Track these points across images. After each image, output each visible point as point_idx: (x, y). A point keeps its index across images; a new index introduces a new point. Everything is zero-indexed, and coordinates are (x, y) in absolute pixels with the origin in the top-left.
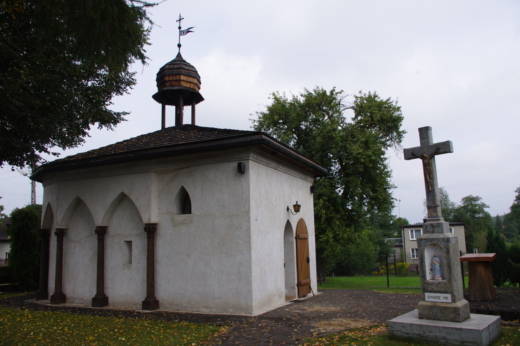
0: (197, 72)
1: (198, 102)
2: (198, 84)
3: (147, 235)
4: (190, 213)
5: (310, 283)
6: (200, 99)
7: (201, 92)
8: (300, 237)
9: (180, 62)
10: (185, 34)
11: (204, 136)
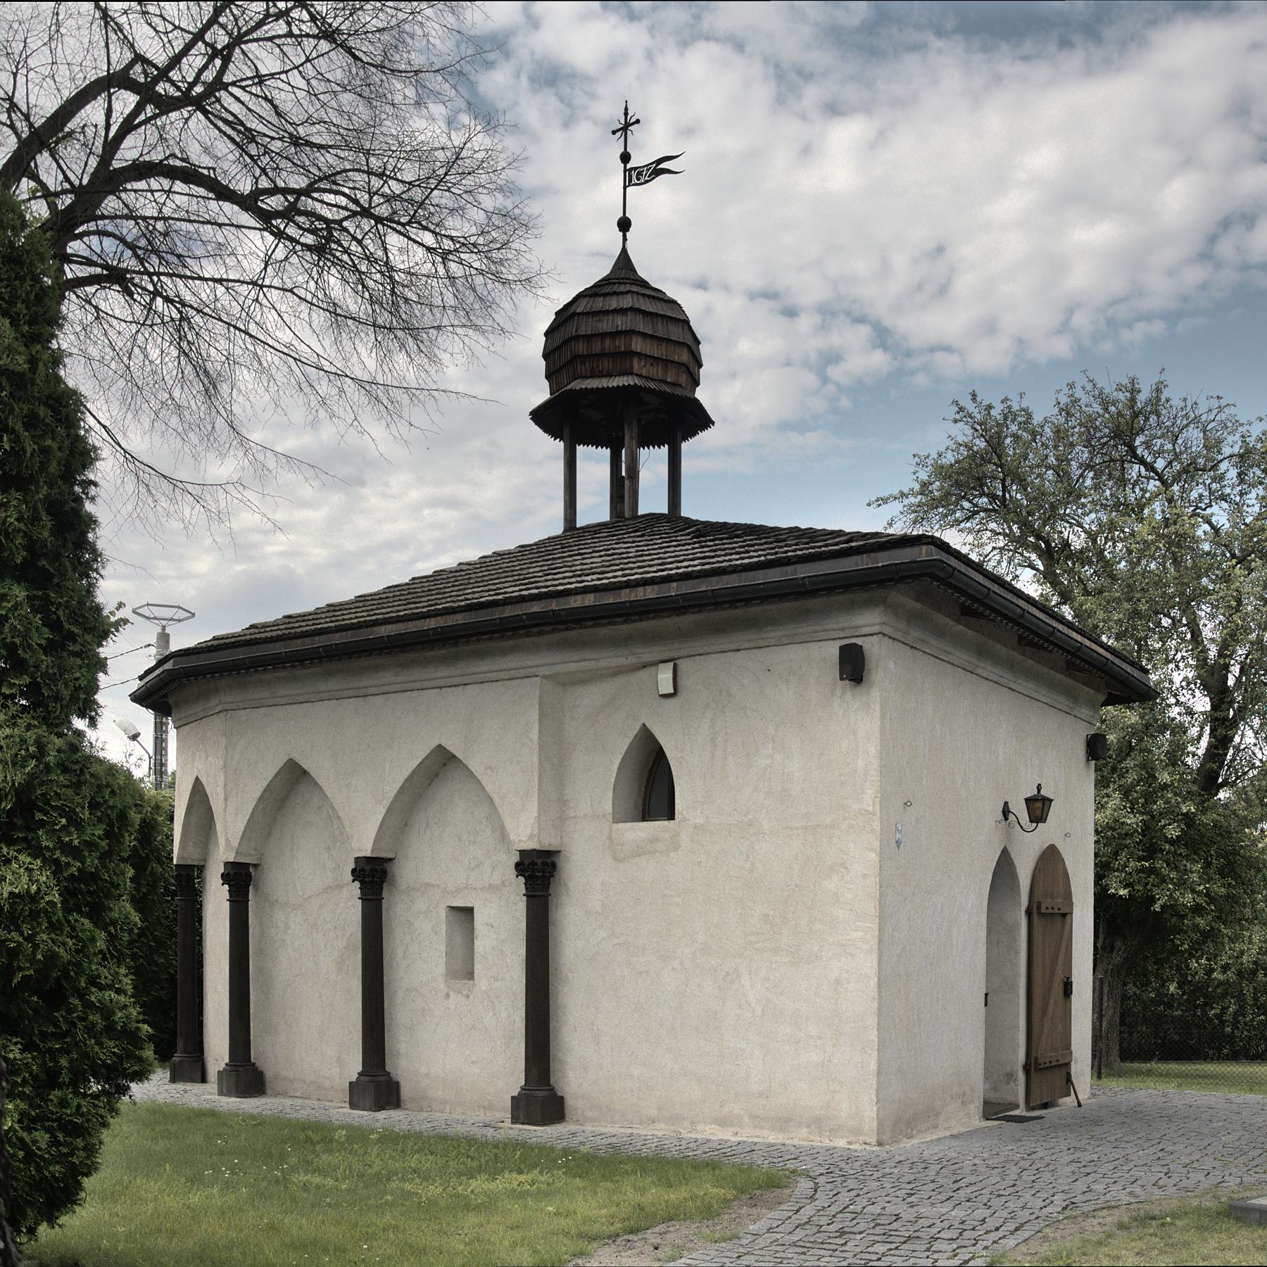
0: (686, 322)
1: (691, 433)
2: (692, 366)
3: (526, 889)
4: (671, 816)
5: (1068, 1065)
6: (699, 420)
7: (701, 394)
8: (1043, 910)
9: (628, 288)
10: (647, 182)
11: (723, 553)
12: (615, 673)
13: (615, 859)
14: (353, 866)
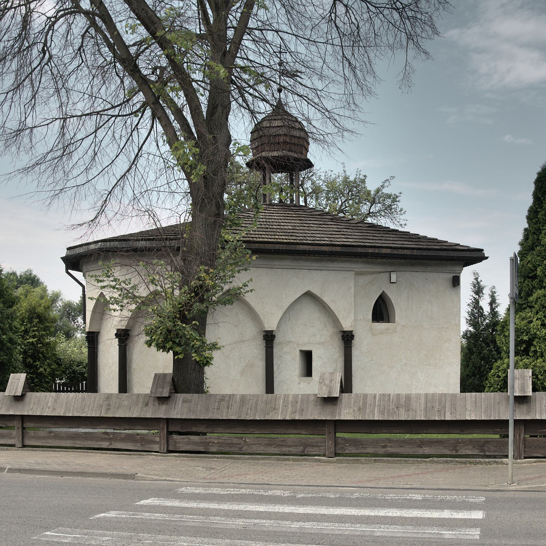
12: (373, 273)
13: (373, 335)
14: (116, 332)
